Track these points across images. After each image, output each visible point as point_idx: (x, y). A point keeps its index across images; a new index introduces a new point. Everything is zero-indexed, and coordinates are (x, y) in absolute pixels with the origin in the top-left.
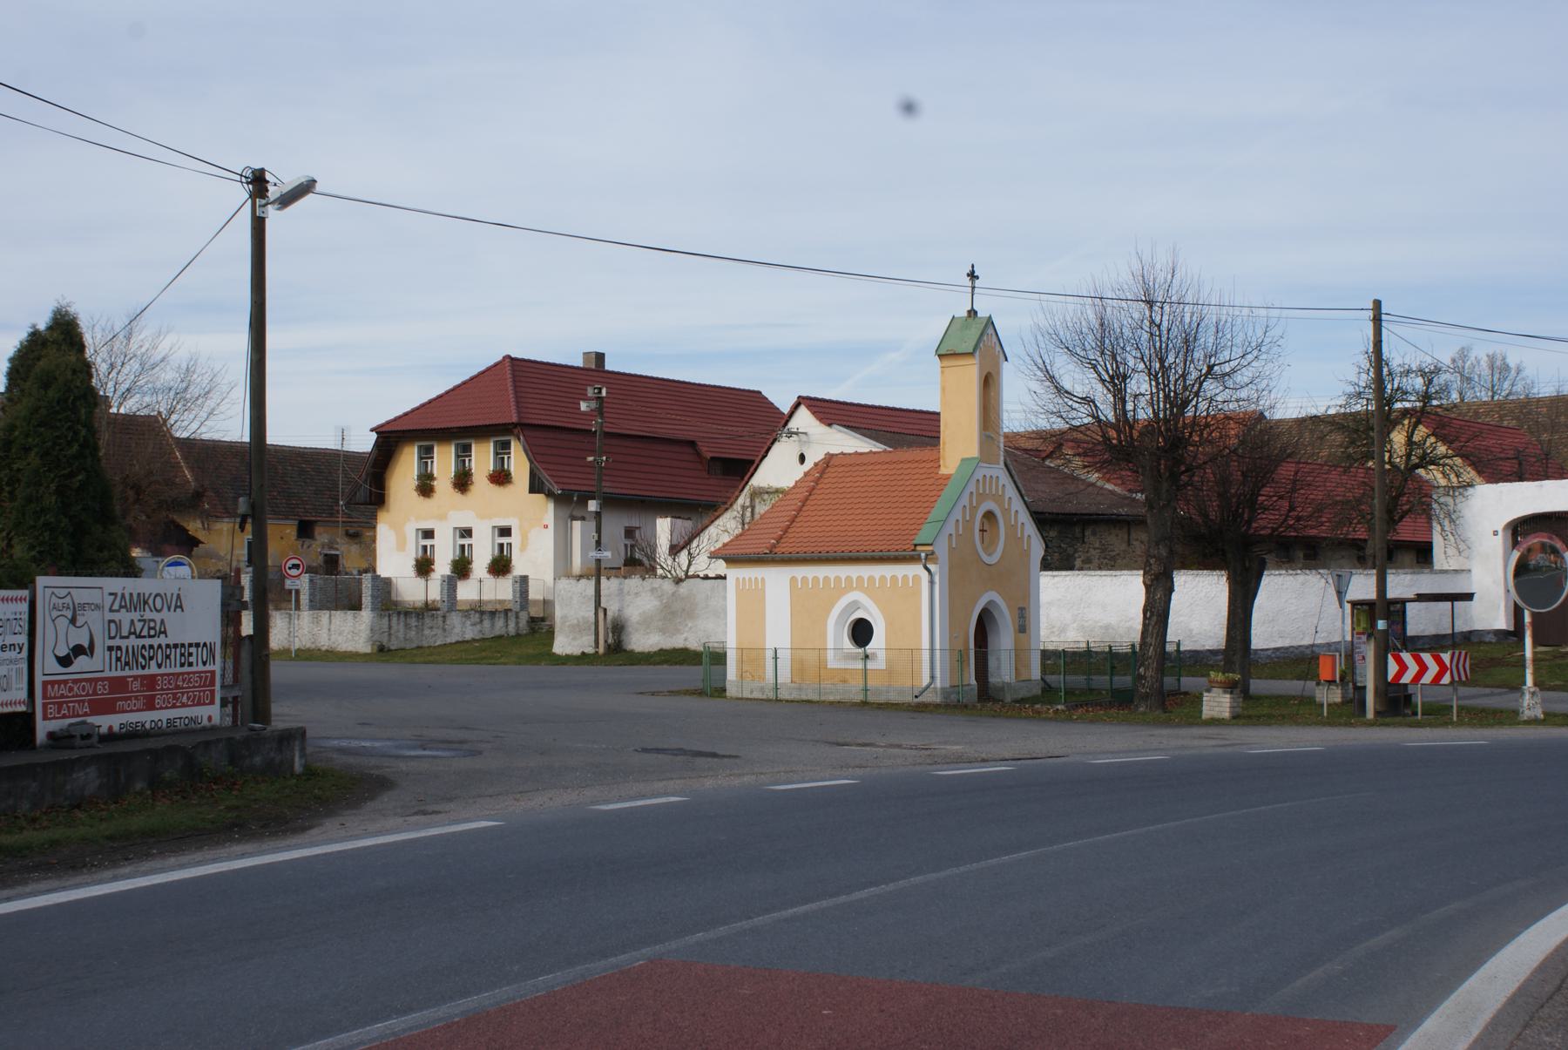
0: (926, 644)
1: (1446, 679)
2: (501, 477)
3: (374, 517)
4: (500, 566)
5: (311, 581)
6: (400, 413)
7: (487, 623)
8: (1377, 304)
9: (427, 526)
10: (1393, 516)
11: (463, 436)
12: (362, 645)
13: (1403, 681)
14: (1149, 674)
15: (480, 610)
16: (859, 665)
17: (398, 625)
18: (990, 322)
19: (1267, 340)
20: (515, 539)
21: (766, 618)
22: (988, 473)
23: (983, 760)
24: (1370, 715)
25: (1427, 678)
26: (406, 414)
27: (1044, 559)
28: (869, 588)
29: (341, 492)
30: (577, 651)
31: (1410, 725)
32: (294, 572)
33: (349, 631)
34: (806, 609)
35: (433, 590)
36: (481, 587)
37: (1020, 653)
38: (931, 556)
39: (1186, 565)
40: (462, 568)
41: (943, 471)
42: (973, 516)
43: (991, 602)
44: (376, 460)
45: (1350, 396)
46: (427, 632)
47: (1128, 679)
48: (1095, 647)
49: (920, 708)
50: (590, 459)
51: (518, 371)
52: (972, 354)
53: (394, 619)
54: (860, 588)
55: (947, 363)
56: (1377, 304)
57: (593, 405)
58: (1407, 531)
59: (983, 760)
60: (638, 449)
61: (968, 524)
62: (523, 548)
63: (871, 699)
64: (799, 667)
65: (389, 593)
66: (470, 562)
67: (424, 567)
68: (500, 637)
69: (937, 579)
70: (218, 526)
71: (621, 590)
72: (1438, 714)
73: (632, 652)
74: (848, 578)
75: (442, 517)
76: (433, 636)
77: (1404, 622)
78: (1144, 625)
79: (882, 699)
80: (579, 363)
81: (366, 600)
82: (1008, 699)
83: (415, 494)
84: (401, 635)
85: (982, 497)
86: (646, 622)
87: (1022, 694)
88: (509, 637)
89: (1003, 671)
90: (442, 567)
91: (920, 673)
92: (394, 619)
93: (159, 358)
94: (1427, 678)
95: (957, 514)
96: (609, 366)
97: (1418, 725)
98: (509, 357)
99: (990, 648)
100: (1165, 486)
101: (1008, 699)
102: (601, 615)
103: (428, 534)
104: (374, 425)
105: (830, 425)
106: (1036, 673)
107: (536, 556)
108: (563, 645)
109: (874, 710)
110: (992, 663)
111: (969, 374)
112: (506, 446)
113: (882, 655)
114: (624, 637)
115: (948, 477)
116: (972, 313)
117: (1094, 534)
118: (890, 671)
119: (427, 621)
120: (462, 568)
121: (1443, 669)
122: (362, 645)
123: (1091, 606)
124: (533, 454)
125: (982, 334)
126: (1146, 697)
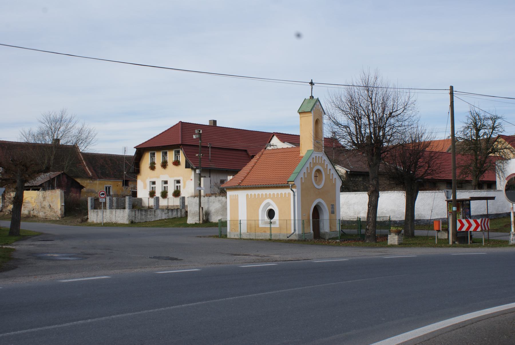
0: (292, 218)
1: (479, 229)
2: (177, 163)
3: (136, 178)
4: (177, 194)
5: (110, 199)
6: (144, 142)
7: (170, 213)
8: (452, 87)
9: (153, 180)
10: (481, 171)
11: (164, 149)
12: (126, 221)
13: (470, 230)
14: (370, 228)
15: (168, 209)
16: (269, 226)
17: (138, 214)
18: (318, 100)
19: (410, 102)
20: (181, 184)
21: (248, 209)
22: (318, 155)
23: (332, 258)
24: (451, 243)
25: (472, 229)
26: (146, 142)
27: (342, 187)
28: (273, 197)
29: (122, 170)
30: (194, 223)
31: (431, 246)
32: (103, 196)
33: (122, 216)
34: (252, 206)
35: (152, 202)
36: (172, 202)
37: (332, 221)
38: (293, 186)
39: (384, 190)
40: (164, 195)
41: (301, 155)
42: (311, 171)
43: (319, 202)
44: (136, 158)
45: (466, 128)
46: (148, 216)
47: (364, 230)
48: (393, 219)
49: (289, 242)
50: (197, 155)
51: (185, 128)
52: (310, 112)
53: (137, 212)
54: (270, 198)
55: (302, 115)
56: (452, 87)
57: (198, 136)
58: (486, 177)
59: (332, 258)
60: (220, 152)
61: (309, 174)
62: (184, 187)
63: (273, 238)
64: (249, 227)
65: (141, 203)
66: (167, 192)
67: (152, 194)
68: (175, 218)
69: (296, 194)
70: (95, 182)
71: (208, 201)
72: (477, 242)
73: (212, 222)
74: (266, 194)
75: (158, 177)
76: (151, 218)
77: (469, 208)
78: (368, 210)
79: (277, 238)
80: (208, 124)
81: (127, 205)
82: (327, 238)
83: (149, 169)
84: (139, 217)
85: (315, 164)
86: (217, 212)
87: (333, 236)
88: (178, 218)
89: (325, 227)
90: (158, 194)
92: (137, 212)
94: (472, 229)
95: (305, 170)
96: (218, 125)
97: (468, 247)
99: (320, 219)
100: (375, 158)
101: (327, 238)
103: (154, 183)
104: (135, 146)
105: (284, 142)
106: (338, 228)
107: (188, 189)
108: (191, 220)
109: (273, 242)
111: (310, 119)
112: (178, 152)
113: (278, 222)
114: (209, 217)
115: (302, 157)
116: (312, 97)
118: (280, 228)
119: (149, 213)
120: (164, 195)
121: (478, 225)
122: (126, 221)
123: (353, 205)
124: (186, 155)
125: (314, 105)
126: (369, 237)
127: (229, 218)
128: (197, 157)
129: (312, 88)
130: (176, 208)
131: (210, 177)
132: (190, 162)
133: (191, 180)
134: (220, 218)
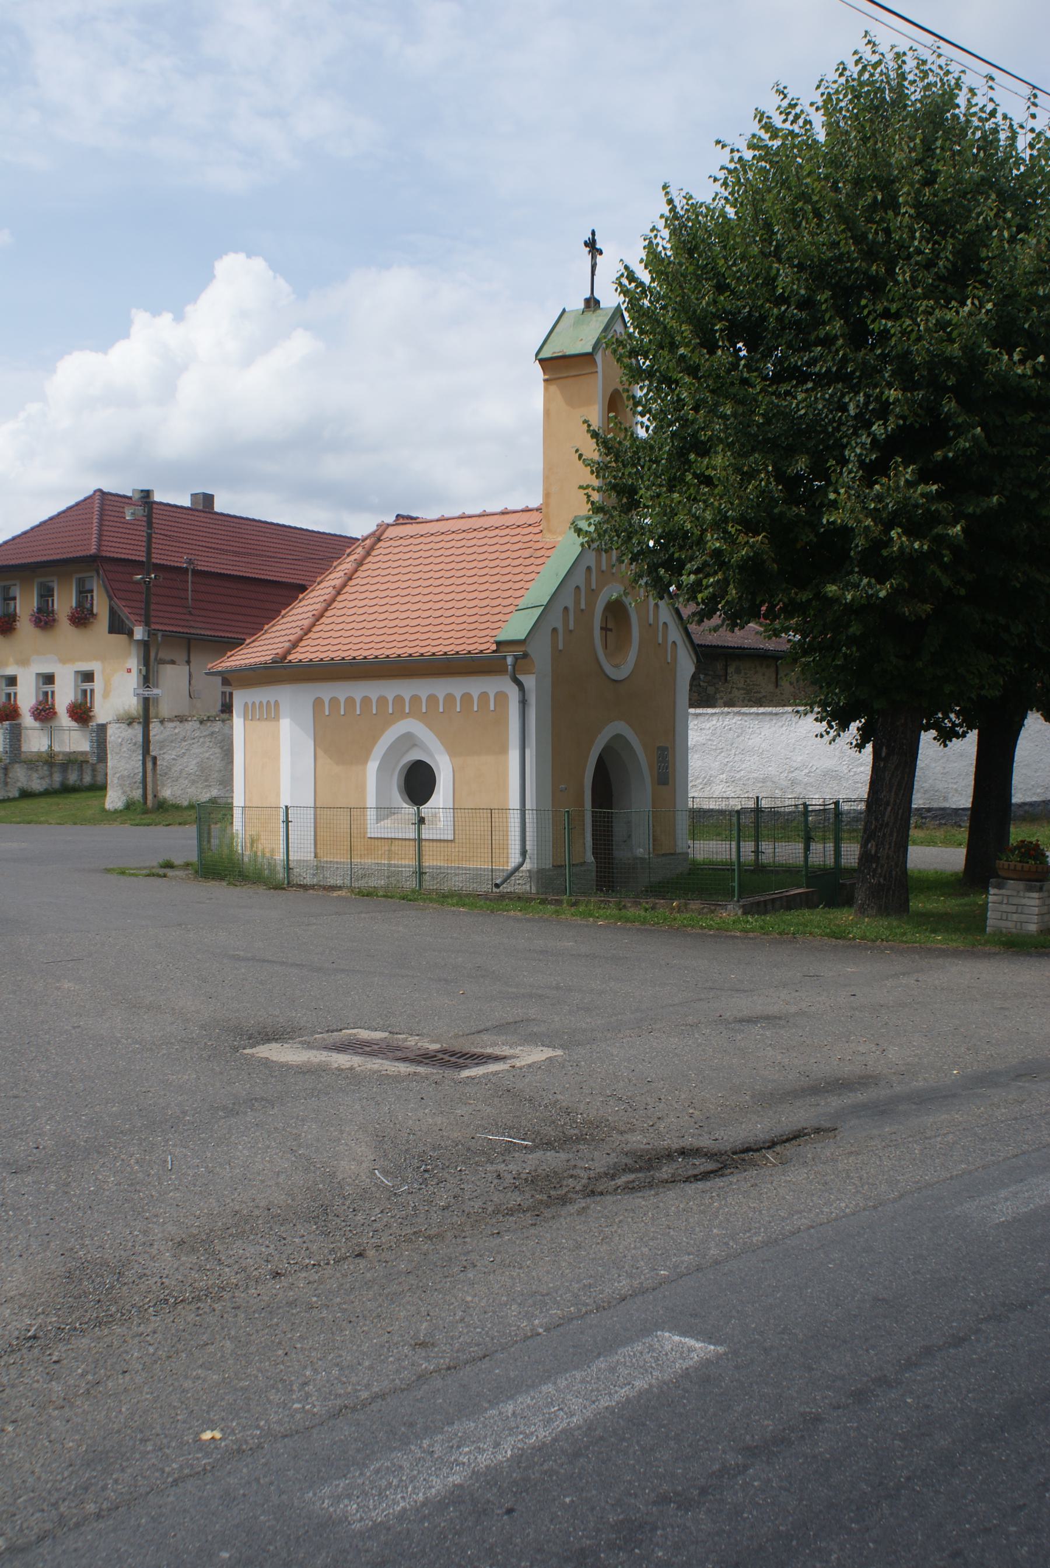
0: (514, 802)
2: (82, 618)
15: (49, 761)
20: (98, 685)
36: (75, 741)
62: (106, 694)
63: (428, 884)
75: (24, 662)
80: (187, 502)
91: (505, 847)
93: (192, 659)
96: (218, 508)
98: (100, 490)
102: (150, 765)
110: (619, 830)
117: (738, 671)
127: (238, 800)
128: (137, 583)
129: (594, 267)
130: (81, 758)
131: (188, 662)
132: (124, 612)
133: (129, 671)
134: (214, 792)
